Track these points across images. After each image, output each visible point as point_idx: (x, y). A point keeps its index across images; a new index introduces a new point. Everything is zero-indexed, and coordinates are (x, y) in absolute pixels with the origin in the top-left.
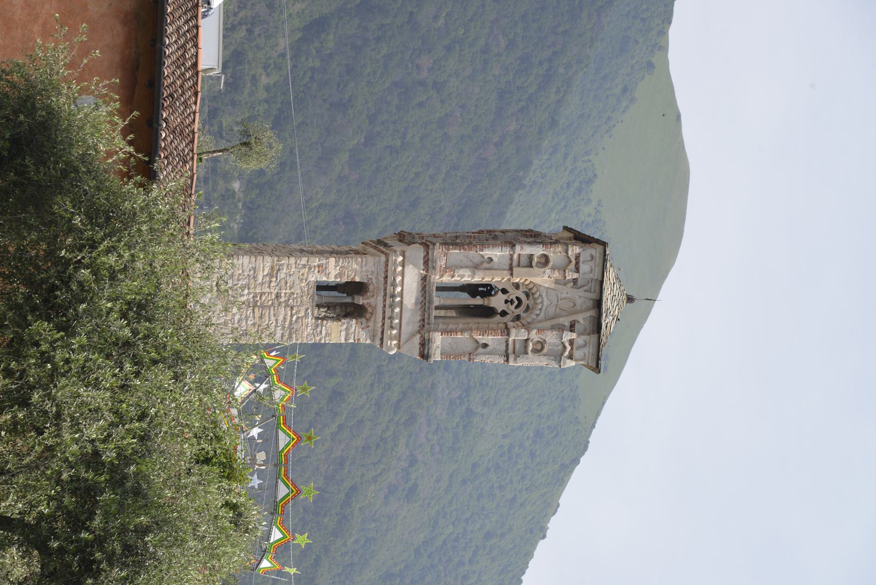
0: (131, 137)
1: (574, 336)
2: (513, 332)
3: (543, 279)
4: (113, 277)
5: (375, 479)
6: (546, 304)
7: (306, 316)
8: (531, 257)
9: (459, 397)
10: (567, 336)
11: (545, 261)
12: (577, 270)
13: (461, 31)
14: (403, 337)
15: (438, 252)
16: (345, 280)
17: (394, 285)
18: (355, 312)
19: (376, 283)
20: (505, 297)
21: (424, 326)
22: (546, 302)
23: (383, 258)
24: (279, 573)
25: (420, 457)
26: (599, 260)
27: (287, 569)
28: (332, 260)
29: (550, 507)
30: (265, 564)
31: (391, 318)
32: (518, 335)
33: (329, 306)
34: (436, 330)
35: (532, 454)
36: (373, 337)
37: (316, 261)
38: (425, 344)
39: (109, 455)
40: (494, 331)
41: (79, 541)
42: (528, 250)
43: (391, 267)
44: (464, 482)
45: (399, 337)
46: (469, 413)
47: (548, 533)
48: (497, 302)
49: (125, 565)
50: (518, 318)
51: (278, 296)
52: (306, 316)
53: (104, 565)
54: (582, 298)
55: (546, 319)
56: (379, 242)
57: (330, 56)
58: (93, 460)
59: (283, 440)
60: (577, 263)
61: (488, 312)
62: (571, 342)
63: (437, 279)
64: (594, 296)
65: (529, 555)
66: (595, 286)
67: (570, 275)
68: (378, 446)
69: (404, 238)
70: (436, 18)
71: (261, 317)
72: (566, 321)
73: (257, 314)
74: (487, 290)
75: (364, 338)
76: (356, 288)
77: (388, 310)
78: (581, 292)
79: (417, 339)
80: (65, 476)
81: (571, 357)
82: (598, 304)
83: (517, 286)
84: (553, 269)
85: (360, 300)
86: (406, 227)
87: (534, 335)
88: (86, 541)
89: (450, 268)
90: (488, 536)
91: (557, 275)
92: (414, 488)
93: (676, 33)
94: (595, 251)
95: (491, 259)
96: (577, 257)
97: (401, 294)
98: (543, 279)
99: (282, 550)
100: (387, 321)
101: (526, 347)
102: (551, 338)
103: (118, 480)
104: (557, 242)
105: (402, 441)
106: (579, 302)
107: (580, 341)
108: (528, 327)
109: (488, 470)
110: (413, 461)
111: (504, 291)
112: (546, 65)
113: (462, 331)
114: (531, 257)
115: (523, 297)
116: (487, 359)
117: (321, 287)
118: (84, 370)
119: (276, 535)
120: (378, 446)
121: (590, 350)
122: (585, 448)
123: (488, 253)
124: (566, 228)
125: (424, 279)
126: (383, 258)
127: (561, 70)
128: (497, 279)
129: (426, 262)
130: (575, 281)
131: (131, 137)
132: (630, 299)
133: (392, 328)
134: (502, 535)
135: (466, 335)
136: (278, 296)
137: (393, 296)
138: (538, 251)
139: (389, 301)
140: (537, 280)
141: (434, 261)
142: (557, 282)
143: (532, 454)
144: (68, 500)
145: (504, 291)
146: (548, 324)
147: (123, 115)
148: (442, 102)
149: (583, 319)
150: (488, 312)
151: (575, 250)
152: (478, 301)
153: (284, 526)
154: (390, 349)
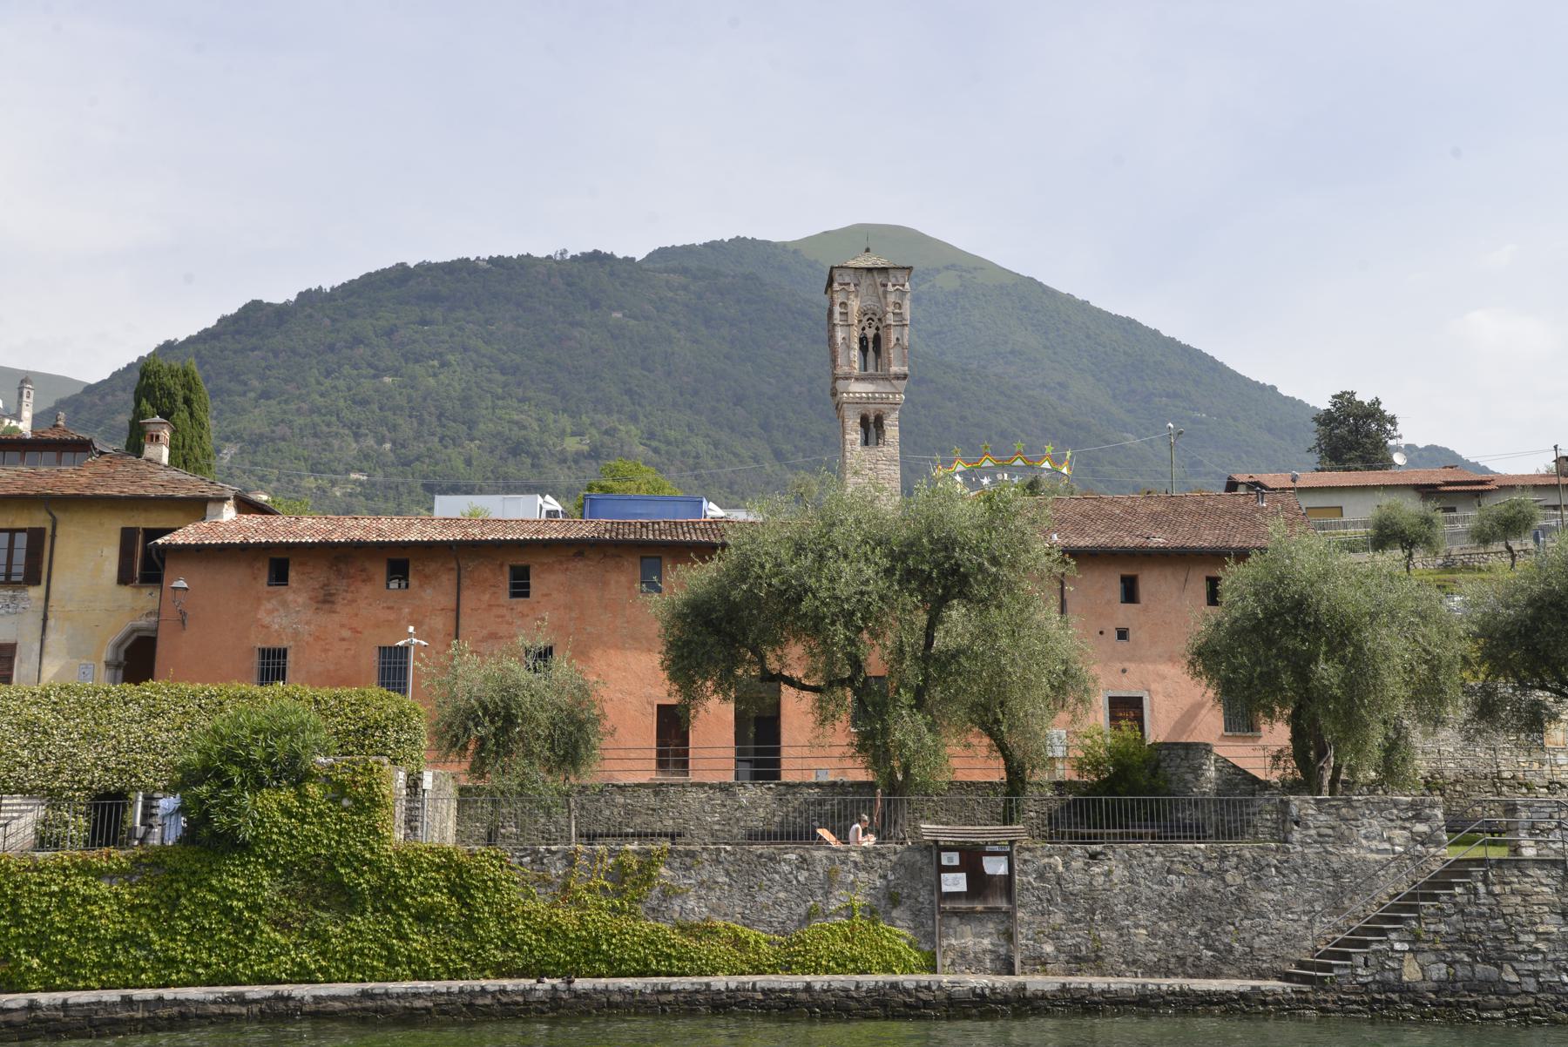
0: (707, 558)
1: (890, 284)
2: (888, 322)
3: (855, 305)
4: (780, 565)
5: (1055, 409)
6: (870, 302)
7: (881, 451)
8: (841, 313)
9: (1002, 358)
10: (890, 288)
11: (843, 304)
12: (849, 284)
13: (777, 368)
14: (894, 390)
15: (839, 371)
16: (859, 428)
17: (861, 398)
18: (879, 421)
19: (861, 409)
20: (867, 328)
21: (886, 378)
22: (869, 303)
23: (845, 405)
24: (1070, 463)
25: (1040, 381)
26: (842, 271)
27: (1068, 457)
28: (847, 437)
29: (1069, 299)
30: (1065, 470)
31: (882, 399)
32: (890, 319)
33: (878, 438)
34: (889, 370)
35: (1037, 311)
36: (894, 410)
37: (848, 447)
38: (898, 377)
39: (886, 563)
40: (888, 334)
41: (938, 577)
42: (837, 316)
43: (850, 400)
44: (1055, 353)
45: (894, 393)
46: (1012, 352)
47: (1086, 299)
48: (870, 333)
49: (954, 549)
50: (880, 320)
51: (871, 469)
52: (881, 451)
53: (953, 562)
54: (866, 281)
55: (880, 302)
56: (837, 408)
57: (795, 447)
58: (889, 572)
59: (987, 464)
60: (845, 284)
61: (877, 338)
62: (894, 285)
63: (856, 372)
64: (865, 272)
65: (1099, 311)
66: (859, 272)
67: (852, 288)
68: (1034, 408)
69: (834, 393)
70: (770, 384)
71: (884, 479)
72: (881, 289)
73: (882, 481)
74: (863, 341)
75: (896, 415)
76: (864, 421)
77: (878, 401)
78: (862, 281)
79: (895, 382)
80: (897, 588)
81: (903, 285)
82: (869, 270)
83: (860, 321)
84: (848, 299)
85: (872, 418)
86: (828, 392)
87: (891, 308)
88: (938, 573)
89: (850, 363)
90: (1088, 337)
91: (852, 297)
92: (1059, 384)
93: (775, 239)
94: (836, 273)
95: (844, 338)
96: (841, 284)
97: (867, 393)
98: (855, 305)
99: (1058, 461)
100: (884, 401)
101: (898, 314)
102: (891, 298)
103: (902, 557)
104: (832, 297)
105: (1030, 393)
106: (868, 282)
107: (893, 280)
108: (885, 313)
109: (1047, 339)
110: (1043, 386)
111: (864, 329)
112: (796, 315)
113: (889, 354)
114: (841, 313)
115: (867, 317)
116: (906, 338)
117: (866, 443)
118: (832, 580)
119: (1046, 465)
120: (1034, 408)
121: (899, 274)
122: (1032, 279)
123: (839, 340)
124: (826, 293)
125: (857, 379)
126: (845, 405)
127: (799, 306)
128: (856, 334)
129: (847, 379)
130: (855, 285)
131: (707, 558)
132: (868, 250)
133: (888, 398)
134: (1088, 328)
135: (891, 351)
136: (871, 469)
137: (868, 398)
138: (837, 309)
139: (871, 401)
140: (856, 309)
141: (846, 374)
142: (856, 296)
143: (1037, 311)
144: (914, 584)
145: (864, 329)
146: (883, 300)
147: (694, 562)
148: (820, 377)
149: (879, 279)
150: (877, 338)
151: (836, 286)
152: (871, 345)
153: (1040, 460)
154: (901, 398)
